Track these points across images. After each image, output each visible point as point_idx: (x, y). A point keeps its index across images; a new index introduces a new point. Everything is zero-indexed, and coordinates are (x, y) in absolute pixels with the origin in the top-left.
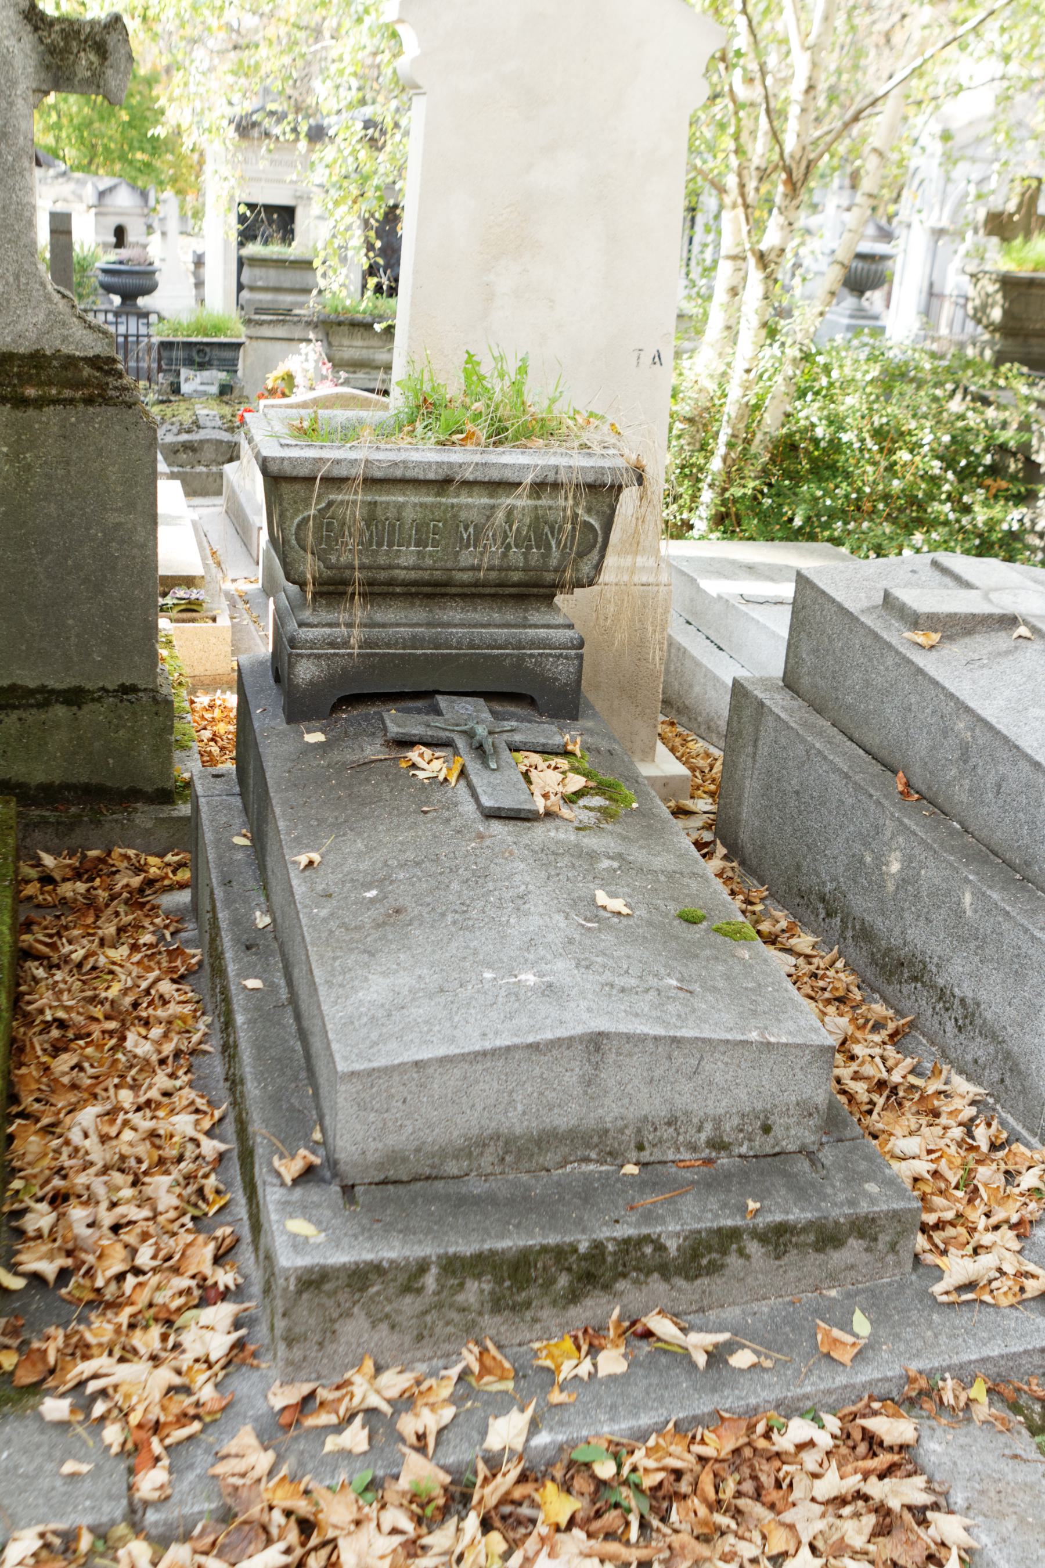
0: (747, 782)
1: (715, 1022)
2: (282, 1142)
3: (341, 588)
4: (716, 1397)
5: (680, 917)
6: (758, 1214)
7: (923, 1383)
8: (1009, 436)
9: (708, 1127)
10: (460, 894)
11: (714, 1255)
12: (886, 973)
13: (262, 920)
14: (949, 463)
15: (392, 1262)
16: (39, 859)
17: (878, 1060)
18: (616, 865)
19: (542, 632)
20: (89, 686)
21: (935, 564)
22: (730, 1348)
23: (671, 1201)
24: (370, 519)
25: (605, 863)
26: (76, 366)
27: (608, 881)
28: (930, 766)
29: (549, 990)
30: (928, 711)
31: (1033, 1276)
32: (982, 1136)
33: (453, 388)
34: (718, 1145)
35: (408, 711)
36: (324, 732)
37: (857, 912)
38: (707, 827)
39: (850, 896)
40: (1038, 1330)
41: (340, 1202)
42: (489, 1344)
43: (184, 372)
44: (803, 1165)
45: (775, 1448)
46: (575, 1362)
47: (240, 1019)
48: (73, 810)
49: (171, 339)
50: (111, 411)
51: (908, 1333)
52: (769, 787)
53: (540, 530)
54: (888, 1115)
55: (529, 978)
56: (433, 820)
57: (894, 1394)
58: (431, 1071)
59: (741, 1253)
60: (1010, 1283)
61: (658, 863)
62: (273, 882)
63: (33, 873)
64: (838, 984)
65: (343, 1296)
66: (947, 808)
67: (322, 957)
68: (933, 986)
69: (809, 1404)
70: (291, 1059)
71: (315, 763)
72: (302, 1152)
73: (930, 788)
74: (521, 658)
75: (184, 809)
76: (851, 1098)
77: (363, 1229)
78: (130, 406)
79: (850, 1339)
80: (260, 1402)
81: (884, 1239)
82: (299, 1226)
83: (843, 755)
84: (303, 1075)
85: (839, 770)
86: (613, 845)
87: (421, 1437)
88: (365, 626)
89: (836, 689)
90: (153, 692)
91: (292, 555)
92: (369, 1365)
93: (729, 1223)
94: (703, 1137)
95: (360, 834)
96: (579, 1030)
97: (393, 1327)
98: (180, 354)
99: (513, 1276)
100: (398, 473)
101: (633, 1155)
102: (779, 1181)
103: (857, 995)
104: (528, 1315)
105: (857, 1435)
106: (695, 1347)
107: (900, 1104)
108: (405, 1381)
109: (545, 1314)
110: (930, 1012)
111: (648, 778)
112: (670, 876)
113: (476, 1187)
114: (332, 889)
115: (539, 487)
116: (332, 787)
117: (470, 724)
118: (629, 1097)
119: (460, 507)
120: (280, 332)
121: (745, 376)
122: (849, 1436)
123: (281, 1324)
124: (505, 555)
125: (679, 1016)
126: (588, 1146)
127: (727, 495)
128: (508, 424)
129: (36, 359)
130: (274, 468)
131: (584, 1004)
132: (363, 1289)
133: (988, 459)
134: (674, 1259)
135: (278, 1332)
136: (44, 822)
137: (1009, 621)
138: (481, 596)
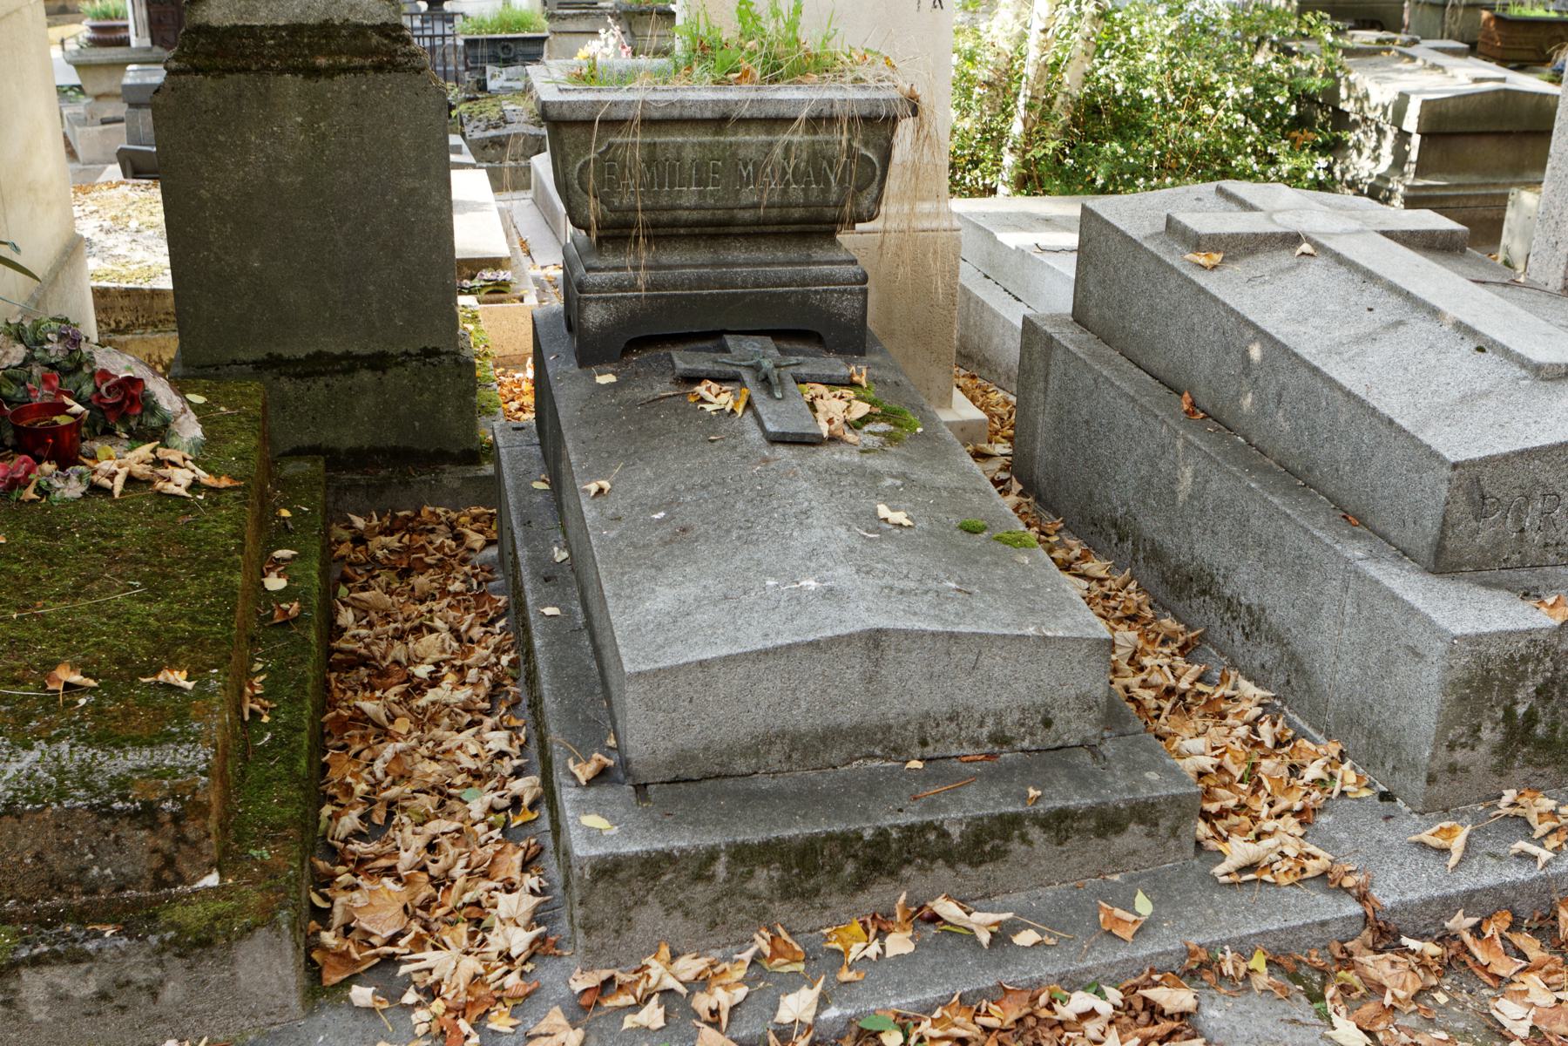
0: (1040, 417)
1: (994, 619)
2: (578, 749)
3: (626, 231)
4: (1000, 973)
5: (961, 527)
6: (1044, 805)
7: (1203, 956)
8: (1316, 83)
9: (990, 721)
10: (744, 512)
11: (997, 842)
12: (1176, 591)
13: (560, 555)
14: (1253, 114)
15: (682, 851)
16: (351, 522)
17: (1166, 668)
18: (899, 482)
19: (826, 269)
20: (392, 351)
21: (1220, 190)
22: (1013, 927)
23: (953, 791)
24: (651, 161)
25: (889, 482)
26: (364, 35)
27: (891, 499)
28: (1215, 384)
29: (830, 593)
30: (1211, 329)
31: (1315, 857)
32: (1266, 731)
33: (729, 31)
34: (1000, 739)
35: (698, 350)
36: (614, 373)
37: (1147, 533)
38: (1004, 469)
39: (1140, 519)
40: (1318, 905)
41: (633, 799)
42: (780, 930)
43: (490, 69)
44: (1085, 757)
45: (1058, 1017)
46: (863, 944)
47: (537, 643)
48: (382, 473)
49: (475, 36)
50: (400, 76)
51: (1189, 911)
52: (1060, 420)
53: (818, 163)
54: (1175, 719)
55: (811, 584)
56: (720, 448)
57: (1175, 968)
58: (715, 670)
59: (1024, 839)
60: (1291, 864)
61: (940, 480)
62: (568, 515)
63: (346, 535)
64: (1129, 604)
65: (637, 885)
66: (1231, 424)
67: (610, 573)
68: (1221, 598)
69: (1092, 977)
70: (587, 677)
71: (606, 402)
72: (596, 755)
73: (1214, 406)
74: (806, 295)
75: (488, 469)
76: (1139, 704)
77: (655, 822)
78: (418, 71)
79: (1131, 917)
80: (562, 988)
81: (1165, 824)
82: (593, 821)
83: (1128, 380)
84: (598, 690)
85: (1127, 395)
86: (897, 466)
87: (714, 1012)
88: (651, 268)
89: (1123, 318)
90: (455, 354)
91: (575, 199)
92: (665, 952)
93: (1011, 809)
94: (985, 731)
95: (648, 463)
96: (858, 627)
97: (687, 915)
98: (485, 51)
99: (800, 864)
100: (676, 113)
101: (917, 751)
102: (1060, 772)
103: (1149, 614)
104: (817, 902)
105: (1139, 1005)
106: (978, 924)
107: (1188, 710)
108: (700, 964)
109: (833, 901)
110: (1219, 623)
111: (947, 423)
112: (952, 492)
113: (764, 783)
114: (622, 512)
115: (817, 121)
116: (623, 423)
117: (757, 359)
118: (910, 694)
119: (738, 145)
120: (584, 25)
121: (1042, 36)
122: (1131, 1007)
123: (579, 912)
124: (785, 192)
125: (957, 614)
126: (872, 742)
127: (1028, 156)
128: (782, 61)
129: (326, 29)
130: (553, 113)
131: (863, 605)
132: (655, 877)
133: (1293, 111)
134: (959, 845)
135: (576, 921)
136: (353, 486)
137: (1291, 240)
138: (764, 235)
